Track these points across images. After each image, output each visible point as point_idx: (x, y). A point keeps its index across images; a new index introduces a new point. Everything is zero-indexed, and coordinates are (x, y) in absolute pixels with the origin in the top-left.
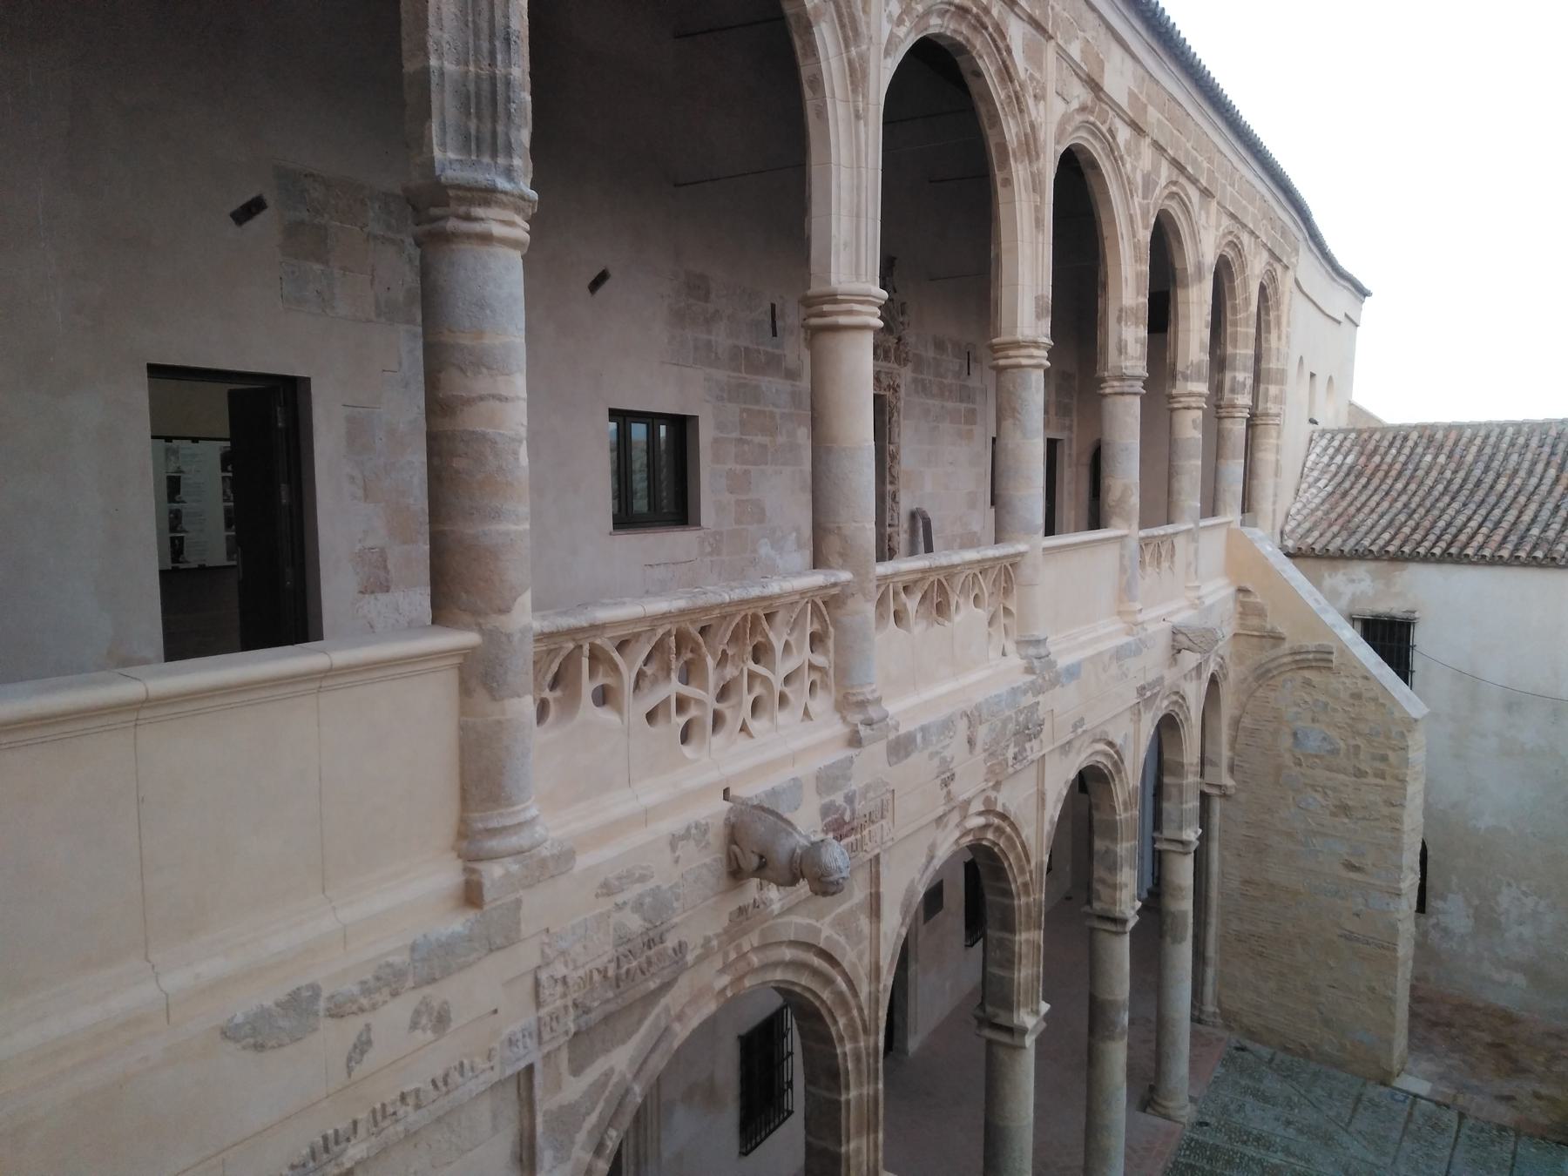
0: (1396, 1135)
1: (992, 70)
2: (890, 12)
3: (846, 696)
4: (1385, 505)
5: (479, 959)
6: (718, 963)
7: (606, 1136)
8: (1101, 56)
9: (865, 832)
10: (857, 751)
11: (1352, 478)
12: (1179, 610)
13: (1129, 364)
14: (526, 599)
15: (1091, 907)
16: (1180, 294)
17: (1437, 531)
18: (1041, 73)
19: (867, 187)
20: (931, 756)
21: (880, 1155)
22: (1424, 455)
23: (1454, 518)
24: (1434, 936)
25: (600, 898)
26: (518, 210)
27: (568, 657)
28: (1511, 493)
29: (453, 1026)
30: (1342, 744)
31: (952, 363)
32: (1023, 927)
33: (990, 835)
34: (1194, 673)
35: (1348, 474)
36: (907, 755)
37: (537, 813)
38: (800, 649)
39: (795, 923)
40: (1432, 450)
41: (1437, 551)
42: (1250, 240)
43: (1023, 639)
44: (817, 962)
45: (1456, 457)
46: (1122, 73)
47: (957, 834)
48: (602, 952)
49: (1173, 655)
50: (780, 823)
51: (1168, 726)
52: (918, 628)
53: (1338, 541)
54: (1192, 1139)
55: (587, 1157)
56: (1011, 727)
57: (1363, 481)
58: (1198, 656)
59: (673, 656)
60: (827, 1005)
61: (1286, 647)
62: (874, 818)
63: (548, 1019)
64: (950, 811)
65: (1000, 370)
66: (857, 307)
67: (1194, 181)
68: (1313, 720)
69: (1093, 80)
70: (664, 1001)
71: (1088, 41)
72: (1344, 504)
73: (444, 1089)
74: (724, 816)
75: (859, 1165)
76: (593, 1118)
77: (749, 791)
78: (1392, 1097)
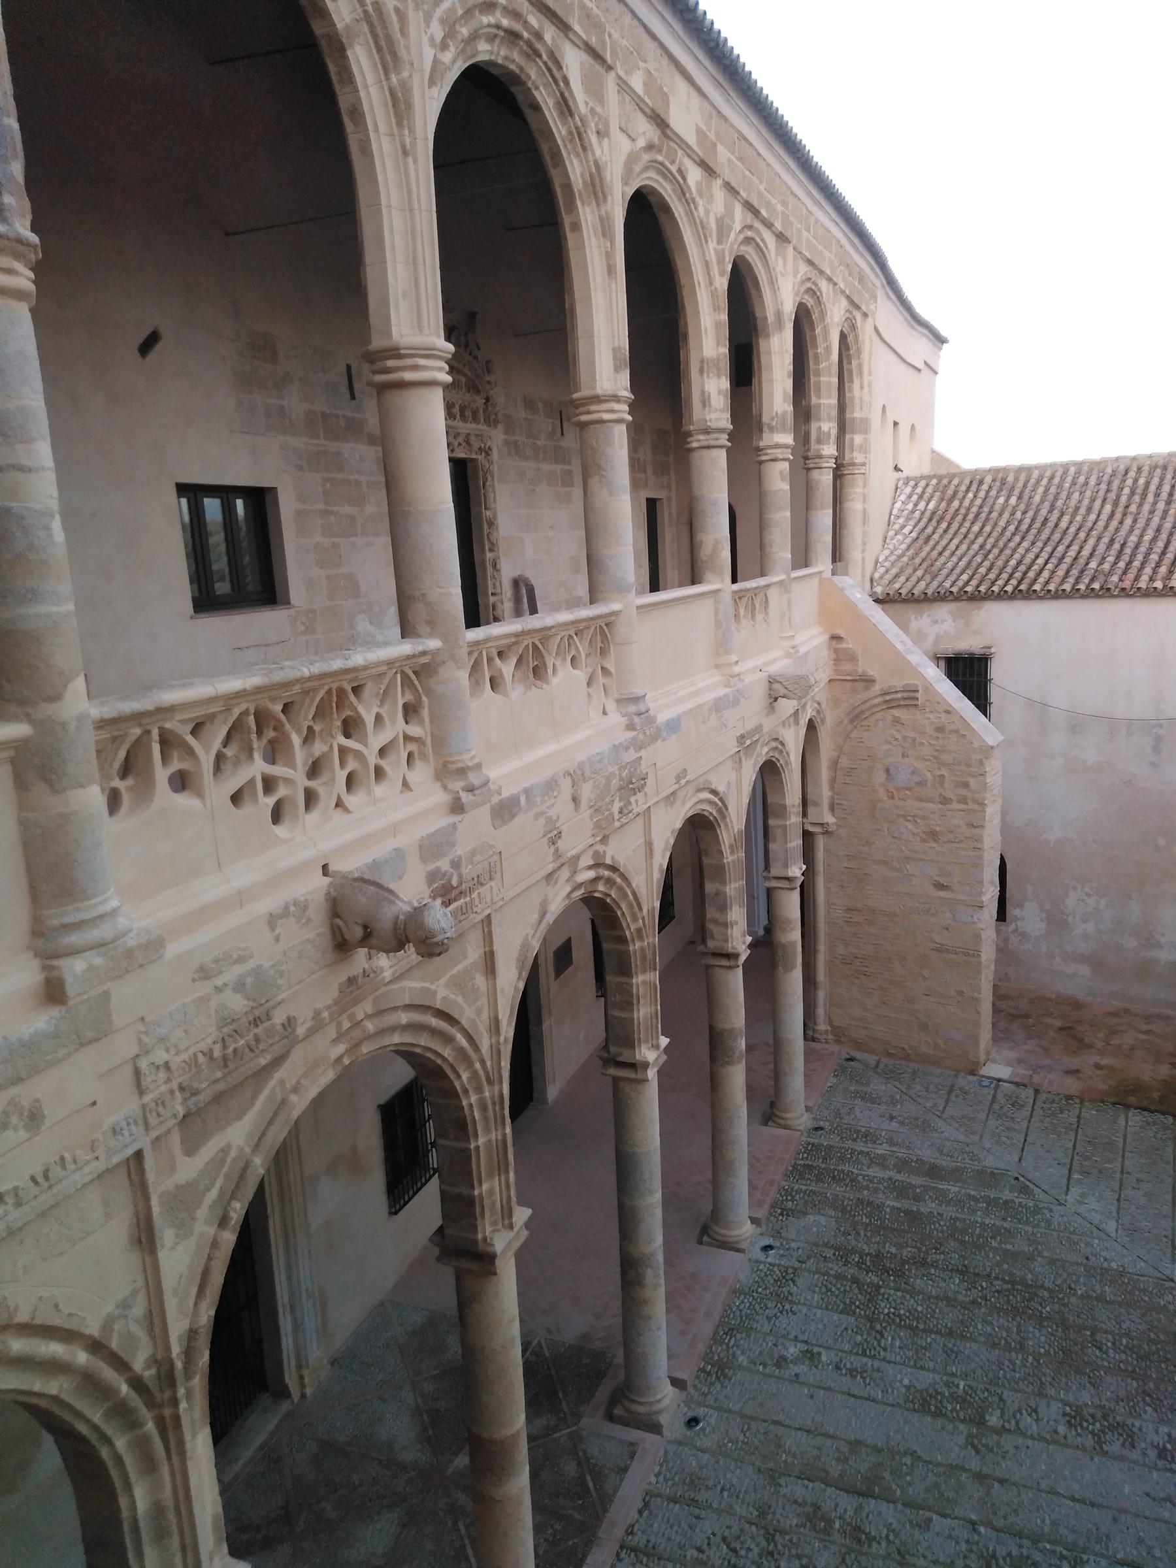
0: (982, 1116)
1: (551, 103)
2: (432, 35)
3: (445, 765)
4: (964, 547)
5: (69, 1054)
6: (332, 1032)
7: (229, 1209)
8: (665, 89)
9: (474, 895)
10: (460, 817)
11: (934, 523)
12: (775, 660)
13: (713, 416)
14: (79, 685)
15: (706, 945)
16: (762, 343)
17: (1009, 570)
18: (603, 106)
19: (422, 232)
20: (537, 816)
21: (513, 1193)
22: (997, 498)
23: (1023, 556)
24: (1014, 940)
25: (197, 983)
26: (18, 256)
27: (138, 741)
28: (1072, 530)
29: (48, 1122)
30: (929, 775)
31: (545, 424)
32: (639, 970)
33: (601, 887)
34: (792, 720)
35: (930, 520)
36: (512, 817)
37: (119, 904)
38: (393, 721)
39: (410, 988)
40: (1004, 493)
41: (1009, 588)
42: (828, 288)
43: (622, 697)
44: (434, 1022)
45: (1026, 497)
46: (688, 108)
47: (568, 889)
48: (206, 1033)
49: (771, 704)
50: (382, 892)
51: (770, 771)
52: (516, 692)
53: (922, 585)
54: (809, 1144)
55: (212, 1230)
56: (615, 783)
57: (944, 525)
58: (795, 702)
59: (254, 736)
60: (448, 1061)
61: (877, 688)
62: (482, 879)
63: (153, 1104)
64: (559, 868)
65: (583, 426)
66: (422, 362)
67: (769, 226)
68: (903, 756)
69: (658, 116)
70: (277, 1076)
71: (650, 73)
72: (927, 548)
73: (46, 1184)
74: (324, 892)
75: (493, 1204)
76: (214, 1194)
77: (349, 865)
78: (980, 1085)
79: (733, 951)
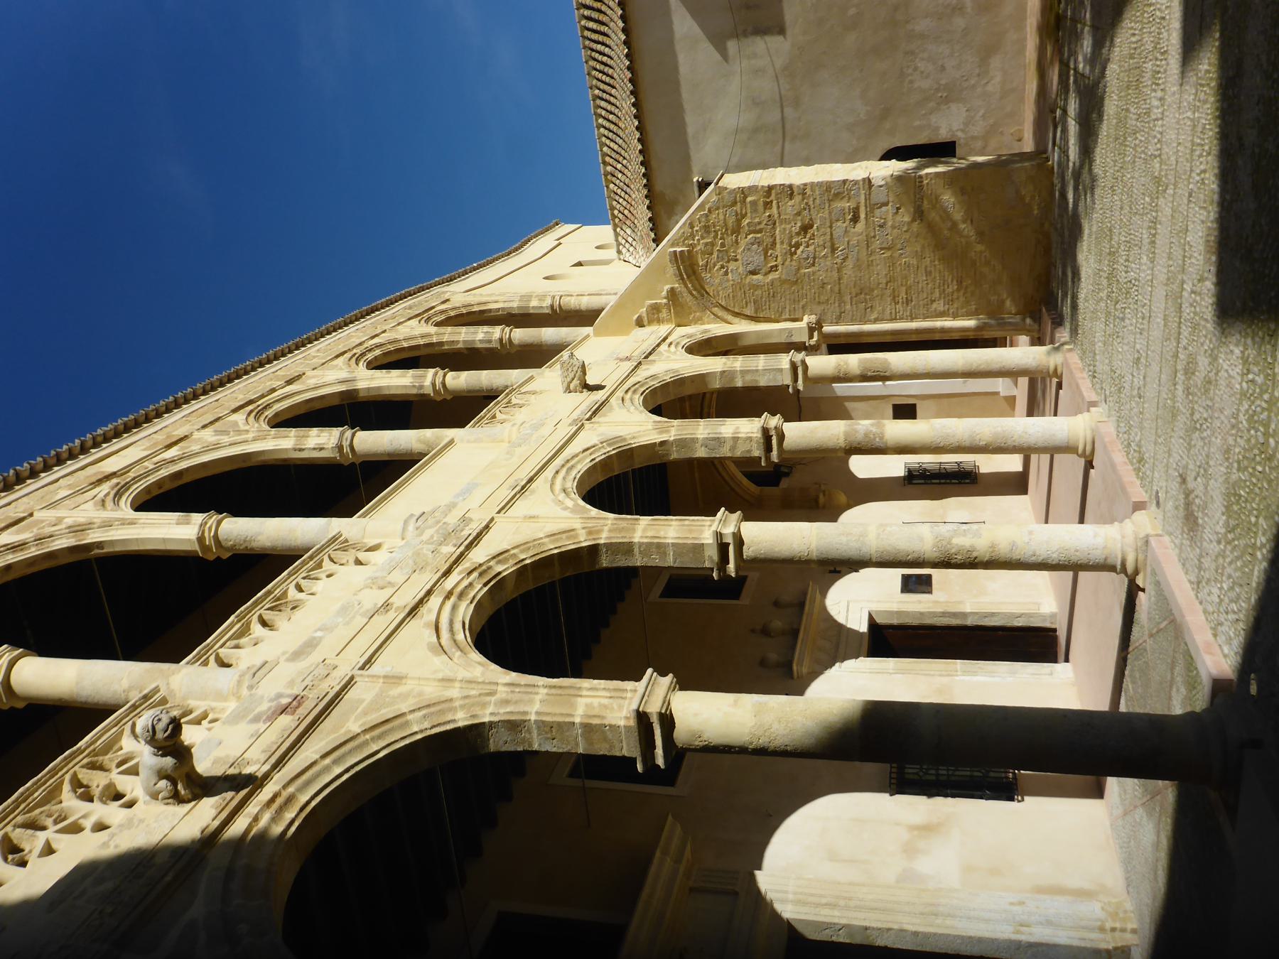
1: (11, 556)
79: (760, 432)
